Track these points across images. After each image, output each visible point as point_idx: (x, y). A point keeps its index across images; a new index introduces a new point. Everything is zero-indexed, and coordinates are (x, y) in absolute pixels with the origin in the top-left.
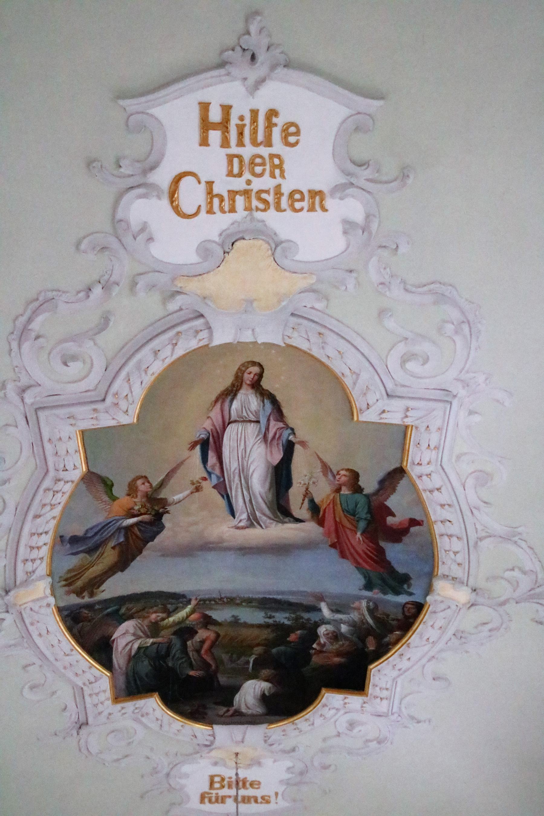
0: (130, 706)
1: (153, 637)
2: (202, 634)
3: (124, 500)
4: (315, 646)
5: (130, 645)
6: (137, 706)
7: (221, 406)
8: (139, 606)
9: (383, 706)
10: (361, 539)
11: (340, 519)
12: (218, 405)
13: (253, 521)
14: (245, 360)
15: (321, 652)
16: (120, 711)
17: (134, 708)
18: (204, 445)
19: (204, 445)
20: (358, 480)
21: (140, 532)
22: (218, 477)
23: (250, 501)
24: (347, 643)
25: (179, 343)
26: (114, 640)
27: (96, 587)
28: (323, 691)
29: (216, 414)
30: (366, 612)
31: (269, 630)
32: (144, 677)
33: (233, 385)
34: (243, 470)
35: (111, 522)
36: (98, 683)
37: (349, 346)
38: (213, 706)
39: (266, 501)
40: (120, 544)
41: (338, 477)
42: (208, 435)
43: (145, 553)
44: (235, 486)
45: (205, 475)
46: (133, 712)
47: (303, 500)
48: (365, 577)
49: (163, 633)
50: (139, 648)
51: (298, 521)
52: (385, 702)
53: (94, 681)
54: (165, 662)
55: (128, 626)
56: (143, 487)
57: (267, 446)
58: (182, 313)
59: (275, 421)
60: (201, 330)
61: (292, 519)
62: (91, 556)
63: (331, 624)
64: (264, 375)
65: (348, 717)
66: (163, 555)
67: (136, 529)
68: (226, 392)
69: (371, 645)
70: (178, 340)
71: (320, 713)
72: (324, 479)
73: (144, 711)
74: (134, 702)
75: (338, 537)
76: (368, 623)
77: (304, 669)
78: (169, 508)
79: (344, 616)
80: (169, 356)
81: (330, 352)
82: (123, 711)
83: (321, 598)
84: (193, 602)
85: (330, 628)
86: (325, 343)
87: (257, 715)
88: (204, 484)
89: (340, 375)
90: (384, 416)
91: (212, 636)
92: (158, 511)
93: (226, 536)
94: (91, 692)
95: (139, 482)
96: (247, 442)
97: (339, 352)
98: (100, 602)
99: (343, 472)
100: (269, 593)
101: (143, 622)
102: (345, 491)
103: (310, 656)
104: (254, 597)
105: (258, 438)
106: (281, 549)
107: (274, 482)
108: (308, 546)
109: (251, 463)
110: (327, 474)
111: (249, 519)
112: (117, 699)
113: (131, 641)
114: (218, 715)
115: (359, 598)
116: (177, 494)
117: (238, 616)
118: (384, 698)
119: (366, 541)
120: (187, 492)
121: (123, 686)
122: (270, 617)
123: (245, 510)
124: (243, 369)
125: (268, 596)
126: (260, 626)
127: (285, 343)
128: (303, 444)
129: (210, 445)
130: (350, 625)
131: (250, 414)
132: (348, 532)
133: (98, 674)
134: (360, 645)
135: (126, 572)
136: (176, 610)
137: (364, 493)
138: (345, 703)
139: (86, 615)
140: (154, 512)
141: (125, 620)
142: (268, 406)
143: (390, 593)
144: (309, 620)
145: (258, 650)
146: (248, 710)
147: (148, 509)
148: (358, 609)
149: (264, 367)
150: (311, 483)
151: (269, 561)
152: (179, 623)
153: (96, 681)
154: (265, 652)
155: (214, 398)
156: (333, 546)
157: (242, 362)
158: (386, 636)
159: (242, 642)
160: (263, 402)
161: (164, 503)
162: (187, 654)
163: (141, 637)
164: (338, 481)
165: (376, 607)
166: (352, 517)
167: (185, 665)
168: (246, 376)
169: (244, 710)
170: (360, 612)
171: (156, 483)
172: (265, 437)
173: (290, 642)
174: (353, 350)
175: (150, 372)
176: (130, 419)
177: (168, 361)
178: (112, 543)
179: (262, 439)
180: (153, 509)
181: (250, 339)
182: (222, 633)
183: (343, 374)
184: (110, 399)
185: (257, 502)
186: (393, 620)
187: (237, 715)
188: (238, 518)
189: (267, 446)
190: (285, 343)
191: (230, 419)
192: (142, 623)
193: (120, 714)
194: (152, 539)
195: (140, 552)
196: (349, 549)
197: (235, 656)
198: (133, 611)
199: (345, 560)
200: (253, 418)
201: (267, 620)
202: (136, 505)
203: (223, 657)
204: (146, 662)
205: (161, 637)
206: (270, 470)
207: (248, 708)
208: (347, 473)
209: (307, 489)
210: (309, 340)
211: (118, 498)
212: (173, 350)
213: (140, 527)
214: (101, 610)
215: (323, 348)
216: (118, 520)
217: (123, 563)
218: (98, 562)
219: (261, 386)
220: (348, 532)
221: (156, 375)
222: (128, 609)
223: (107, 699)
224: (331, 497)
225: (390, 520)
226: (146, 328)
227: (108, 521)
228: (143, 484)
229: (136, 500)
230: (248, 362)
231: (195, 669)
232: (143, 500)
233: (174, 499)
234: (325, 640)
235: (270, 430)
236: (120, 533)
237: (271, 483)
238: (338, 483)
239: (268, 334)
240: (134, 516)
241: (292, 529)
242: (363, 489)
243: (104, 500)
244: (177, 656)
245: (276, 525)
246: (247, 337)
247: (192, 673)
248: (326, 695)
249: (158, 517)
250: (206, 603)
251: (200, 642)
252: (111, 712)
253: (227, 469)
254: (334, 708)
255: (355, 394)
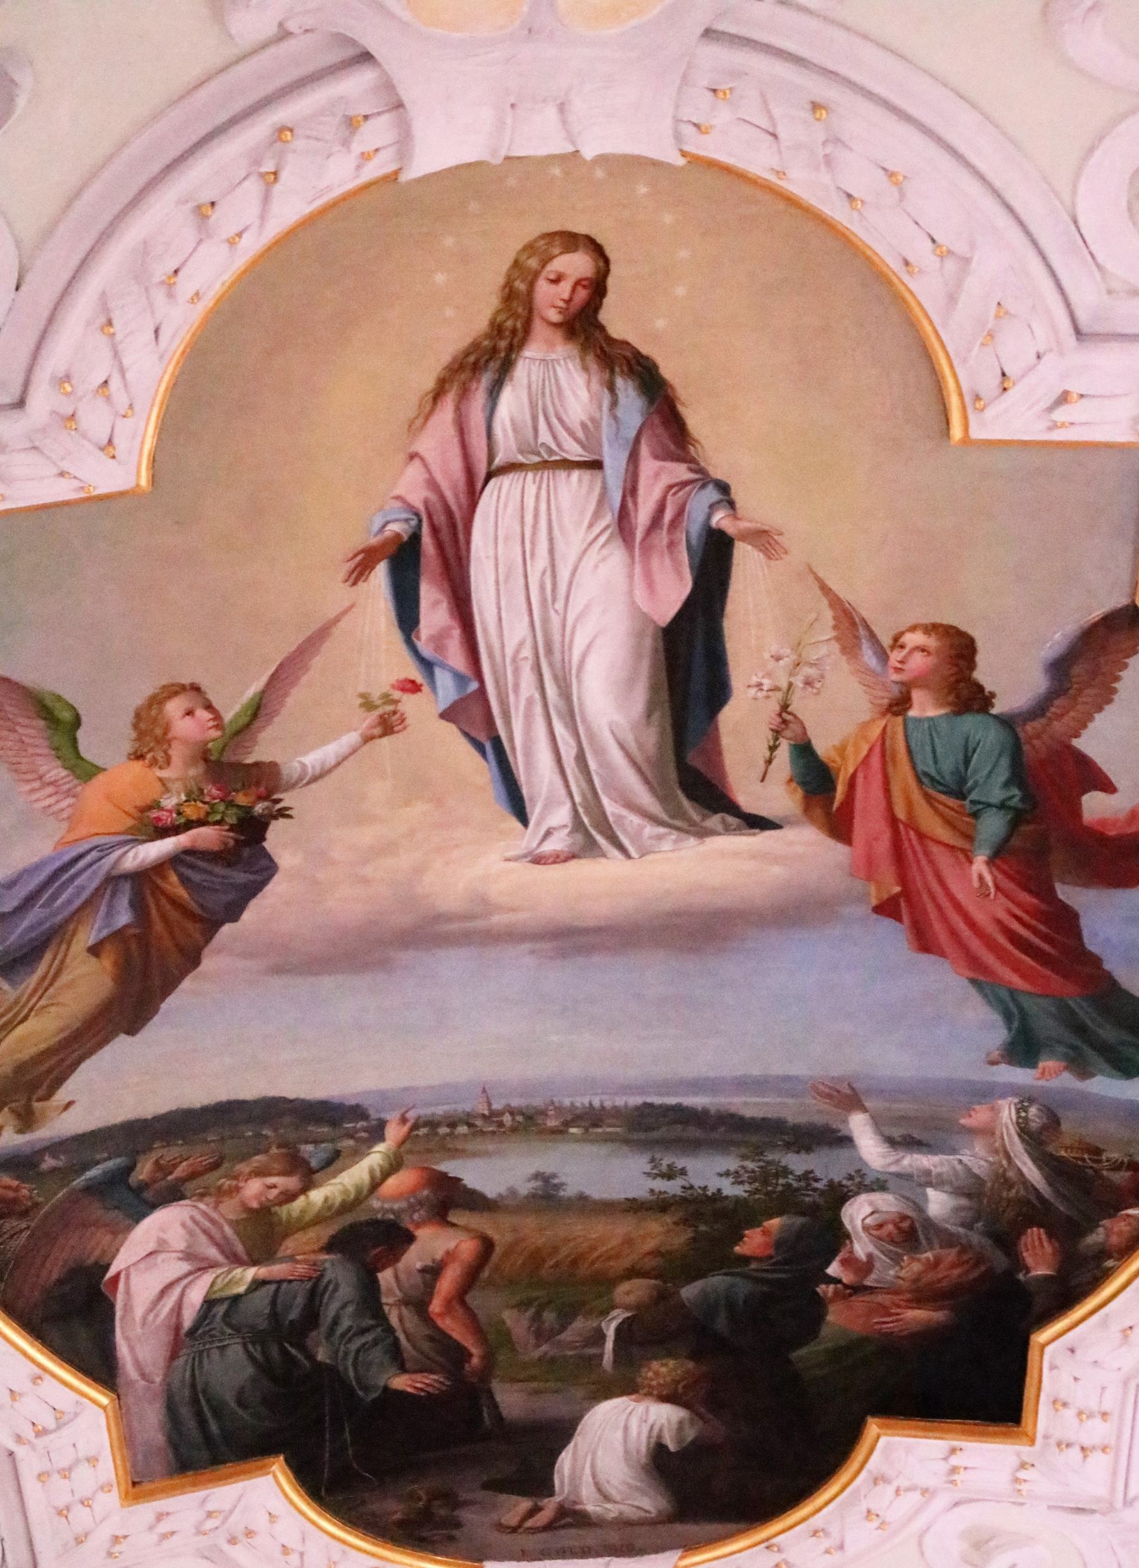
0: (189, 1506)
1: (255, 1263)
2: (432, 1243)
3: (123, 779)
4: (834, 1269)
5: (177, 1291)
6: (210, 1507)
7: (458, 409)
8: (197, 1155)
9: (1092, 1478)
10: (988, 879)
11: (909, 804)
12: (446, 413)
13: (593, 834)
14: (531, 229)
15: (857, 1289)
16: (151, 1528)
17: (201, 1515)
18: (403, 559)
19: (403, 559)
20: (971, 664)
21: (186, 888)
22: (460, 679)
23: (581, 758)
24: (951, 1255)
25: (284, 175)
26: (116, 1278)
27: (41, 1092)
28: (873, 1426)
29: (437, 441)
30: (1016, 1139)
31: (668, 1219)
32: (230, 1399)
33: (496, 329)
34: (549, 650)
35: (81, 856)
36: (65, 1432)
37: (933, 150)
38: (480, 1495)
39: (639, 759)
40: (118, 935)
41: (895, 656)
42: (414, 523)
43: (209, 963)
44: (522, 708)
45: (415, 673)
46: (200, 1532)
47: (773, 749)
48: (1008, 1017)
49: (289, 1246)
50: (209, 1303)
51: (757, 823)
52: (1099, 1462)
53: (51, 1424)
54: (302, 1347)
55: (167, 1224)
56: (186, 726)
57: (632, 557)
58: (290, 45)
59: (656, 457)
60: (366, 117)
61: (731, 819)
62: (13, 984)
63: (895, 1196)
64: (611, 281)
65: (968, 1515)
66: (278, 970)
67: (174, 878)
68: (472, 359)
69: (1039, 1259)
70: (281, 157)
71: (863, 1508)
72: (844, 664)
73: (237, 1522)
74: (201, 1494)
75: (903, 878)
76: (1025, 1182)
77: (802, 1352)
78: (287, 799)
79: (936, 1159)
80: (254, 222)
81: (853, 176)
82: (164, 1527)
83: (850, 1098)
84: (394, 1132)
85: (887, 1203)
86: (837, 140)
87: (641, 1523)
88: (410, 704)
89: (895, 265)
90: (1060, 415)
91: (468, 1247)
92: (248, 809)
93: (498, 891)
94: (45, 1465)
95: (174, 708)
96: (560, 544)
97: (891, 175)
98: (57, 1147)
99: (914, 639)
100: (666, 1087)
101: (216, 1208)
102: (925, 707)
103: (819, 1306)
104: (608, 1104)
105: (597, 529)
106: (698, 931)
107: (663, 675)
108: (794, 913)
109: (577, 620)
110: (858, 646)
111: (578, 825)
112: (138, 1484)
113: (179, 1279)
114: (500, 1527)
115: (987, 1093)
116: (312, 748)
117: (554, 1176)
118: (1094, 1448)
119: (1009, 886)
120: (352, 738)
121: (160, 1439)
122: (670, 1175)
123: (562, 791)
124: (533, 263)
125: (657, 1100)
126: (634, 1207)
127: (684, 154)
128: (763, 538)
129: (423, 560)
130: (958, 1192)
131: (563, 434)
132: (944, 860)
133: (64, 1399)
134: (1000, 1261)
135: (154, 1030)
136: (333, 1162)
137: (994, 711)
138: (954, 1470)
139: (11, 1194)
140: (238, 817)
141: (153, 1207)
142: (632, 403)
143: (1102, 1072)
144: (808, 1176)
145: (633, 1292)
146: (609, 1506)
147: (212, 806)
148: (988, 1132)
149: (609, 251)
150: (798, 681)
151: (654, 973)
152: (347, 1207)
153: (59, 1428)
154: (662, 1297)
155: (429, 383)
156: (887, 909)
157: (527, 239)
158: (1092, 1225)
159: (575, 1263)
160: (611, 388)
161: (266, 780)
162: (380, 1316)
163: (213, 1265)
164: (898, 670)
165: (1053, 1121)
166: (952, 802)
167: (377, 1354)
168: (543, 288)
169: (591, 1505)
170: (996, 1142)
171: (237, 708)
172: (624, 520)
173: (745, 1260)
174: (945, 161)
175: (186, 286)
176: (123, 473)
177: (252, 244)
178: (88, 935)
179: (614, 528)
180: (231, 804)
181: (557, 145)
182: (501, 1238)
183: (907, 263)
184: (42, 401)
185: (605, 764)
186: (1117, 1167)
187: (569, 1526)
188: (538, 824)
189: (632, 557)
190: (684, 154)
191: (491, 457)
192: (215, 1215)
193: (153, 1537)
194: (233, 912)
195: (192, 959)
196: (944, 919)
197: (549, 1317)
198: (179, 1172)
199: (932, 957)
200: (574, 451)
201: (660, 1185)
202: (167, 790)
203: (509, 1322)
204: (236, 1351)
205: (282, 1260)
206: (648, 642)
207: (607, 1498)
208: (931, 642)
209: (785, 707)
210: (774, 136)
211: (98, 770)
212: (266, 199)
213: (189, 873)
214: (63, 1175)
215: (828, 160)
216: (104, 850)
217: (133, 1002)
218: (42, 1002)
219: (602, 328)
220: (944, 860)
221: (207, 302)
222: (162, 1169)
223: (104, 1488)
224: (876, 732)
225: (1095, 806)
226: (155, 117)
227: (66, 858)
228: (190, 713)
229: (164, 774)
230: (550, 236)
231: (408, 1365)
232: (192, 772)
233: (303, 765)
234: (871, 1248)
235: (640, 500)
236: (114, 894)
237: (654, 689)
238: (895, 677)
239: (621, 118)
240: (163, 832)
241: (736, 854)
242: (993, 695)
243: (48, 777)
244: (346, 1323)
245: (676, 842)
246: (540, 137)
247: (401, 1382)
248: (883, 1441)
249: (252, 830)
250: (435, 1132)
251: (424, 1270)
252: (120, 1533)
253: (489, 648)
254: (911, 1489)
255: (953, 334)
